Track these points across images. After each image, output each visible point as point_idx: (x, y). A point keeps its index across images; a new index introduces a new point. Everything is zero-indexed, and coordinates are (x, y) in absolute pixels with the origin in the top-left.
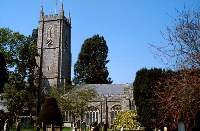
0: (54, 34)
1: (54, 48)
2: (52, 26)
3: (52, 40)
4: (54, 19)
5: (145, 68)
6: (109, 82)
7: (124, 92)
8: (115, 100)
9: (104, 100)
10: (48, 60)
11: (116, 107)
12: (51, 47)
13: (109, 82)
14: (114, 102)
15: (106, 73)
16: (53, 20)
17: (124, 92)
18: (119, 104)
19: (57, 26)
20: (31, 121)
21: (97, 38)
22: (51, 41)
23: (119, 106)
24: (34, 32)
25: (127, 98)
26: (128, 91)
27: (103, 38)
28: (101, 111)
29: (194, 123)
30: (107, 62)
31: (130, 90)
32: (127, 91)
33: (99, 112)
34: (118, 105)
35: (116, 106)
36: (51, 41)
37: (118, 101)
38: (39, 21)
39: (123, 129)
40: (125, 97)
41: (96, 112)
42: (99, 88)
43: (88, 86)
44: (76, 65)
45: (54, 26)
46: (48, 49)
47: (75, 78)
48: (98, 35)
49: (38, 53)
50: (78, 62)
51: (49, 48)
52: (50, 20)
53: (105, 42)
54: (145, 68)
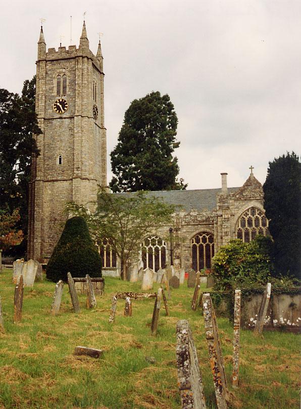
0: (69, 89)
1: (72, 118)
2: (64, 70)
3: (56, 102)
4: (67, 56)
5: (293, 153)
6: (176, 187)
7: (220, 206)
8: (200, 221)
9: (177, 223)
10: (58, 143)
11: (201, 237)
12: (64, 116)
13: (176, 187)
14: (196, 226)
15: (174, 170)
16: (66, 57)
17: (220, 206)
20: (36, 269)
21: (154, 98)
22: (58, 104)
23: (208, 233)
24: (25, 87)
25: (225, 218)
26: (226, 204)
27: (166, 98)
28: (170, 245)
29: (206, 247)
30: (177, 146)
31: (231, 201)
32: (224, 203)
34: (204, 233)
35: (200, 234)
36: (58, 104)
37: (207, 224)
39: (272, 287)
40: (222, 216)
41: (161, 246)
42: (164, 196)
43: (153, 195)
44: (113, 154)
45: (70, 71)
46: (59, 120)
47: (114, 180)
48: (158, 93)
49: (38, 126)
50: (118, 147)
51: (61, 118)
52: (60, 57)
53: (170, 106)
54: (293, 153)
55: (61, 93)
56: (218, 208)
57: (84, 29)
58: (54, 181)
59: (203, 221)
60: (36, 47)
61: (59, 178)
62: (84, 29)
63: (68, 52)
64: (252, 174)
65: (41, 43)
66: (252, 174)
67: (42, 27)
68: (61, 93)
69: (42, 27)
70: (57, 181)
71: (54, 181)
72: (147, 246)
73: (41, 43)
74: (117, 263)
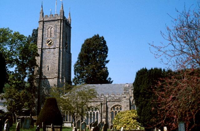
0: (54, 34)
1: (54, 48)
2: (52, 26)
3: (52, 40)
4: (54, 19)
5: (145, 68)
6: (109, 82)
7: (124, 92)
8: (115, 100)
9: (104, 100)
10: (48, 60)
11: (116, 107)
12: (51, 47)
13: (109, 82)
14: (114, 102)
15: (106, 73)
16: (53, 20)
17: (124, 92)
19: (57, 26)
20: (31, 121)
21: (97, 38)
22: (51, 41)
23: (119, 106)
24: (34, 32)
25: (127, 98)
26: (128, 91)
27: (103, 38)
28: (101, 111)
29: (194, 123)
30: (107, 62)
32: (127, 91)
33: (99, 112)
34: (118, 105)
36: (51, 41)
37: (118, 101)
39: (123, 129)
40: (125, 97)
41: (96, 112)
42: (99, 88)
43: (88, 86)
44: (76, 65)
45: (54, 26)
46: (48, 49)
47: (75, 78)
48: (98, 35)
49: (38, 53)
50: (78, 62)
51: (49, 48)
52: (50, 20)
53: (105, 42)
54: (145, 68)
56: (124, 93)
59: (117, 99)
72: (114, 110)
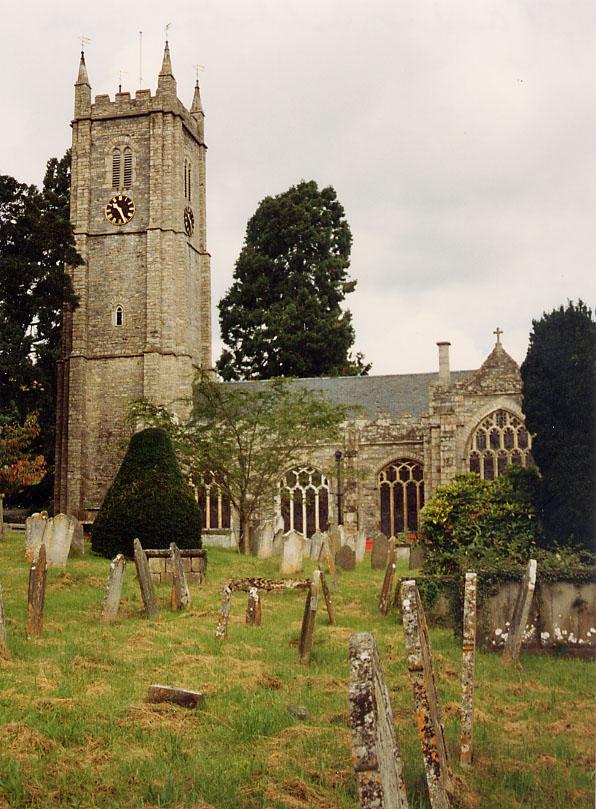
0: (138, 175)
1: (142, 233)
2: (126, 139)
3: (112, 202)
4: (133, 111)
5: (581, 303)
6: (348, 370)
7: (435, 408)
8: (395, 437)
9: (350, 441)
11: (397, 469)
12: (127, 229)
13: (348, 370)
14: (388, 448)
15: (345, 336)
16: (131, 113)
17: (435, 408)
18: (412, 455)
19: (146, 140)
20: (72, 531)
21: (305, 193)
22: (115, 206)
23: (411, 462)
24: (50, 172)
25: (445, 432)
26: (448, 404)
27: (329, 193)
28: (336, 485)
29: (407, 488)
30: (350, 288)
32: (443, 401)
33: (331, 488)
34: (404, 460)
36: (115, 206)
37: (409, 443)
38: (73, 119)
39: (538, 568)
40: (439, 427)
41: (320, 487)
42: (326, 388)
43: (303, 385)
44: (223, 304)
45: (138, 141)
46: (116, 237)
47: (226, 357)
48: (313, 184)
49: (75, 250)
50: (234, 290)
51: (120, 233)
52: (119, 114)
53: (338, 211)
54: (581, 303)
55: (122, 184)
56: (431, 411)
57: (167, 58)
58: (106, 358)
60: (71, 93)
61: (117, 352)
62: (167, 58)
63: (134, 103)
64: (498, 344)
65: (82, 85)
66: (498, 344)
67: (83, 53)
68: (122, 184)
69: (83, 53)
70: (112, 357)
71: (106, 358)
73: (82, 85)
74: (232, 521)
